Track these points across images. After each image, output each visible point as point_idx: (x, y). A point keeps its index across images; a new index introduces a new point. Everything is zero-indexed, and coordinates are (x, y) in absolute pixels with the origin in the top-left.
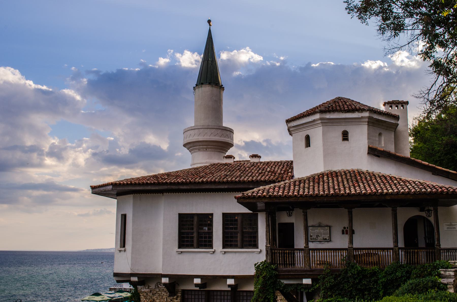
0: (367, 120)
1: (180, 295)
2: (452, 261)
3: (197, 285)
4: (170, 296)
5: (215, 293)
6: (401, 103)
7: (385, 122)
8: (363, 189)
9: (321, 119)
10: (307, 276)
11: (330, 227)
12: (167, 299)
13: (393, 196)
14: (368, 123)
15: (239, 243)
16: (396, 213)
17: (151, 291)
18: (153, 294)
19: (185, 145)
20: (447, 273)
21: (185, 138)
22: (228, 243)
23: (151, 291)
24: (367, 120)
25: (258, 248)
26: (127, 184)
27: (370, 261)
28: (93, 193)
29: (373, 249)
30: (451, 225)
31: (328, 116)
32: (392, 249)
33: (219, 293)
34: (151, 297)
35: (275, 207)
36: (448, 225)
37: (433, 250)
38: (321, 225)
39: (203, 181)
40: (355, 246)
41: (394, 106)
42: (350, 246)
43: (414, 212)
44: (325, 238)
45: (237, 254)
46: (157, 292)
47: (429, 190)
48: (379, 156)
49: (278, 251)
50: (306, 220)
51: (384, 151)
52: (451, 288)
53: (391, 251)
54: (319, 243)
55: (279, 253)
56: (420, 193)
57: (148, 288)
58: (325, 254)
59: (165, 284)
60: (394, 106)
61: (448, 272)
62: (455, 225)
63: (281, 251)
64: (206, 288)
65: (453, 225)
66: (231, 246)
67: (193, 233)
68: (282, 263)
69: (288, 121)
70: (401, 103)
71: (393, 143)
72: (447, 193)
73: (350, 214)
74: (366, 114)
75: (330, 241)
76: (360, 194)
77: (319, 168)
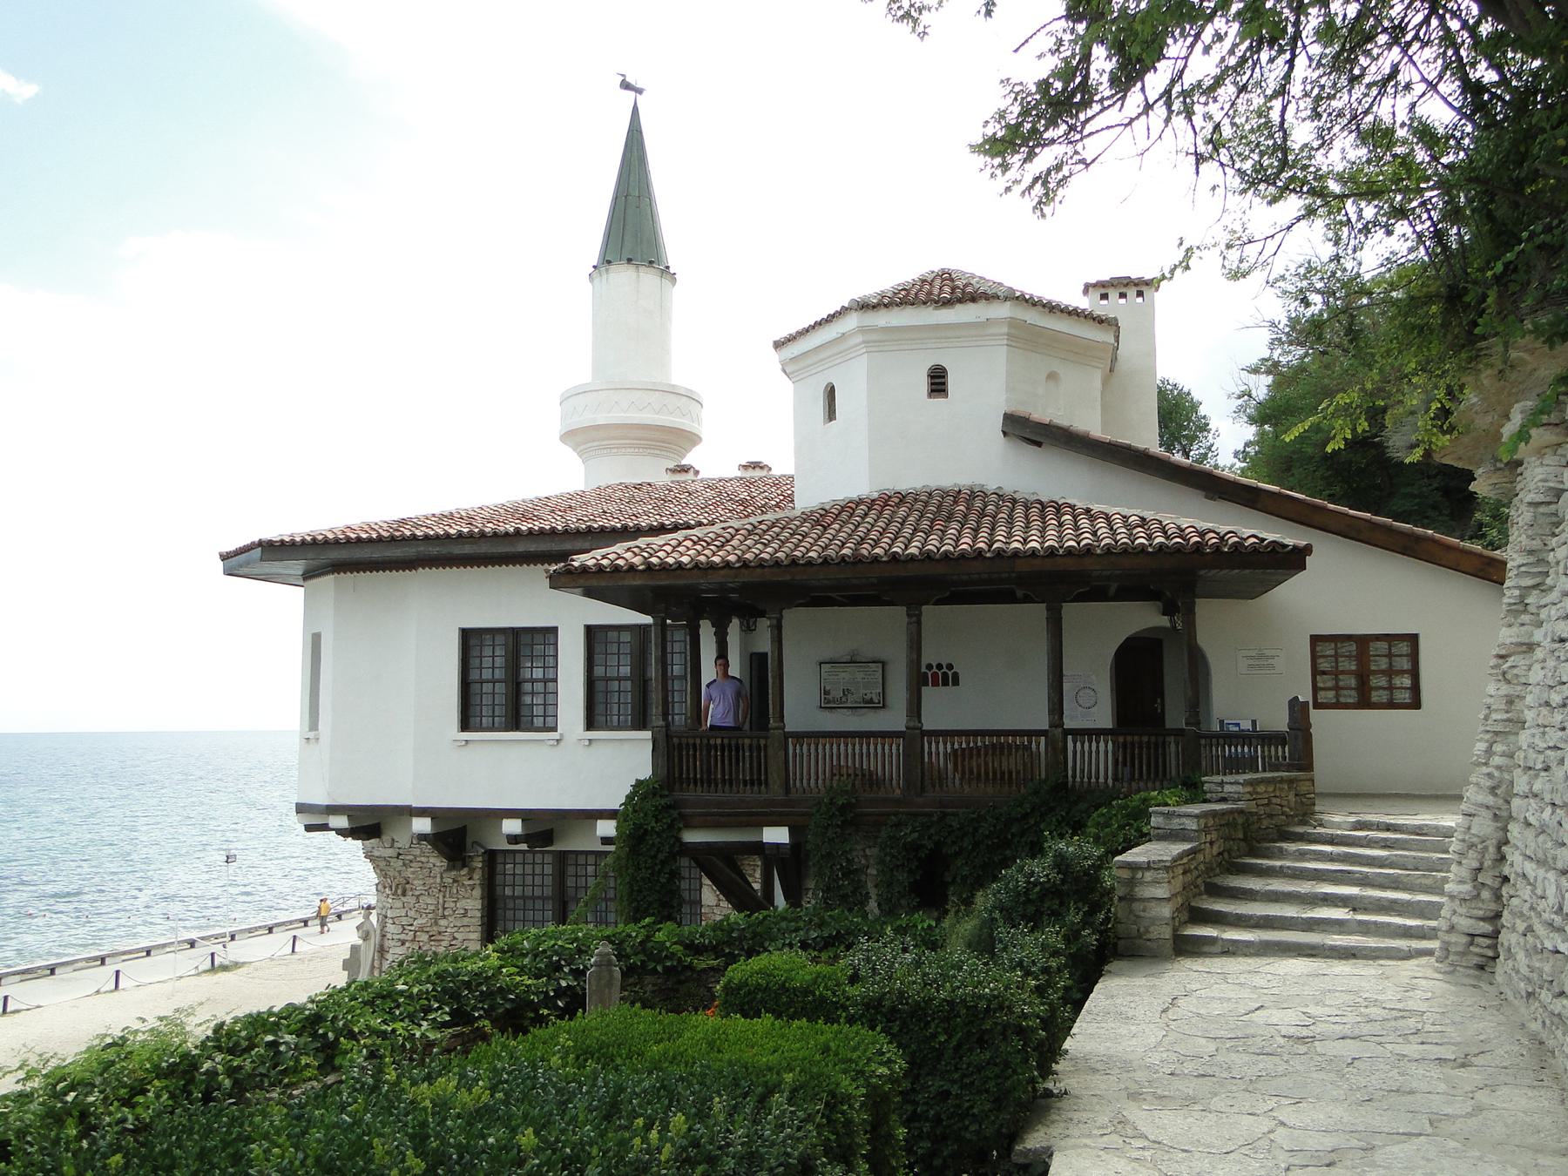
0: (1005, 330)
3: (513, 839)
4: (449, 869)
5: (581, 860)
9: (862, 330)
11: (884, 664)
13: (1037, 562)
24: (1005, 330)
26: (370, 540)
27: (1004, 767)
28: (229, 572)
29: (1015, 733)
30: (1261, 656)
31: (883, 319)
33: (591, 860)
35: (686, 599)
36: (1252, 657)
39: (518, 531)
40: (928, 725)
41: (1113, 294)
43: (1143, 617)
44: (868, 697)
45: (626, 746)
48: (1039, 444)
50: (915, 645)
51: (1110, 444)
52: (1156, 882)
56: (1129, 552)
59: (422, 837)
60: (1113, 294)
65: (1268, 658)
67: (498, 685)
69: (778, 345)
70: (1136, 285)
72: (1217, 549)
74: (1003, 311)
76: (928, 557)
77: (857, 484)
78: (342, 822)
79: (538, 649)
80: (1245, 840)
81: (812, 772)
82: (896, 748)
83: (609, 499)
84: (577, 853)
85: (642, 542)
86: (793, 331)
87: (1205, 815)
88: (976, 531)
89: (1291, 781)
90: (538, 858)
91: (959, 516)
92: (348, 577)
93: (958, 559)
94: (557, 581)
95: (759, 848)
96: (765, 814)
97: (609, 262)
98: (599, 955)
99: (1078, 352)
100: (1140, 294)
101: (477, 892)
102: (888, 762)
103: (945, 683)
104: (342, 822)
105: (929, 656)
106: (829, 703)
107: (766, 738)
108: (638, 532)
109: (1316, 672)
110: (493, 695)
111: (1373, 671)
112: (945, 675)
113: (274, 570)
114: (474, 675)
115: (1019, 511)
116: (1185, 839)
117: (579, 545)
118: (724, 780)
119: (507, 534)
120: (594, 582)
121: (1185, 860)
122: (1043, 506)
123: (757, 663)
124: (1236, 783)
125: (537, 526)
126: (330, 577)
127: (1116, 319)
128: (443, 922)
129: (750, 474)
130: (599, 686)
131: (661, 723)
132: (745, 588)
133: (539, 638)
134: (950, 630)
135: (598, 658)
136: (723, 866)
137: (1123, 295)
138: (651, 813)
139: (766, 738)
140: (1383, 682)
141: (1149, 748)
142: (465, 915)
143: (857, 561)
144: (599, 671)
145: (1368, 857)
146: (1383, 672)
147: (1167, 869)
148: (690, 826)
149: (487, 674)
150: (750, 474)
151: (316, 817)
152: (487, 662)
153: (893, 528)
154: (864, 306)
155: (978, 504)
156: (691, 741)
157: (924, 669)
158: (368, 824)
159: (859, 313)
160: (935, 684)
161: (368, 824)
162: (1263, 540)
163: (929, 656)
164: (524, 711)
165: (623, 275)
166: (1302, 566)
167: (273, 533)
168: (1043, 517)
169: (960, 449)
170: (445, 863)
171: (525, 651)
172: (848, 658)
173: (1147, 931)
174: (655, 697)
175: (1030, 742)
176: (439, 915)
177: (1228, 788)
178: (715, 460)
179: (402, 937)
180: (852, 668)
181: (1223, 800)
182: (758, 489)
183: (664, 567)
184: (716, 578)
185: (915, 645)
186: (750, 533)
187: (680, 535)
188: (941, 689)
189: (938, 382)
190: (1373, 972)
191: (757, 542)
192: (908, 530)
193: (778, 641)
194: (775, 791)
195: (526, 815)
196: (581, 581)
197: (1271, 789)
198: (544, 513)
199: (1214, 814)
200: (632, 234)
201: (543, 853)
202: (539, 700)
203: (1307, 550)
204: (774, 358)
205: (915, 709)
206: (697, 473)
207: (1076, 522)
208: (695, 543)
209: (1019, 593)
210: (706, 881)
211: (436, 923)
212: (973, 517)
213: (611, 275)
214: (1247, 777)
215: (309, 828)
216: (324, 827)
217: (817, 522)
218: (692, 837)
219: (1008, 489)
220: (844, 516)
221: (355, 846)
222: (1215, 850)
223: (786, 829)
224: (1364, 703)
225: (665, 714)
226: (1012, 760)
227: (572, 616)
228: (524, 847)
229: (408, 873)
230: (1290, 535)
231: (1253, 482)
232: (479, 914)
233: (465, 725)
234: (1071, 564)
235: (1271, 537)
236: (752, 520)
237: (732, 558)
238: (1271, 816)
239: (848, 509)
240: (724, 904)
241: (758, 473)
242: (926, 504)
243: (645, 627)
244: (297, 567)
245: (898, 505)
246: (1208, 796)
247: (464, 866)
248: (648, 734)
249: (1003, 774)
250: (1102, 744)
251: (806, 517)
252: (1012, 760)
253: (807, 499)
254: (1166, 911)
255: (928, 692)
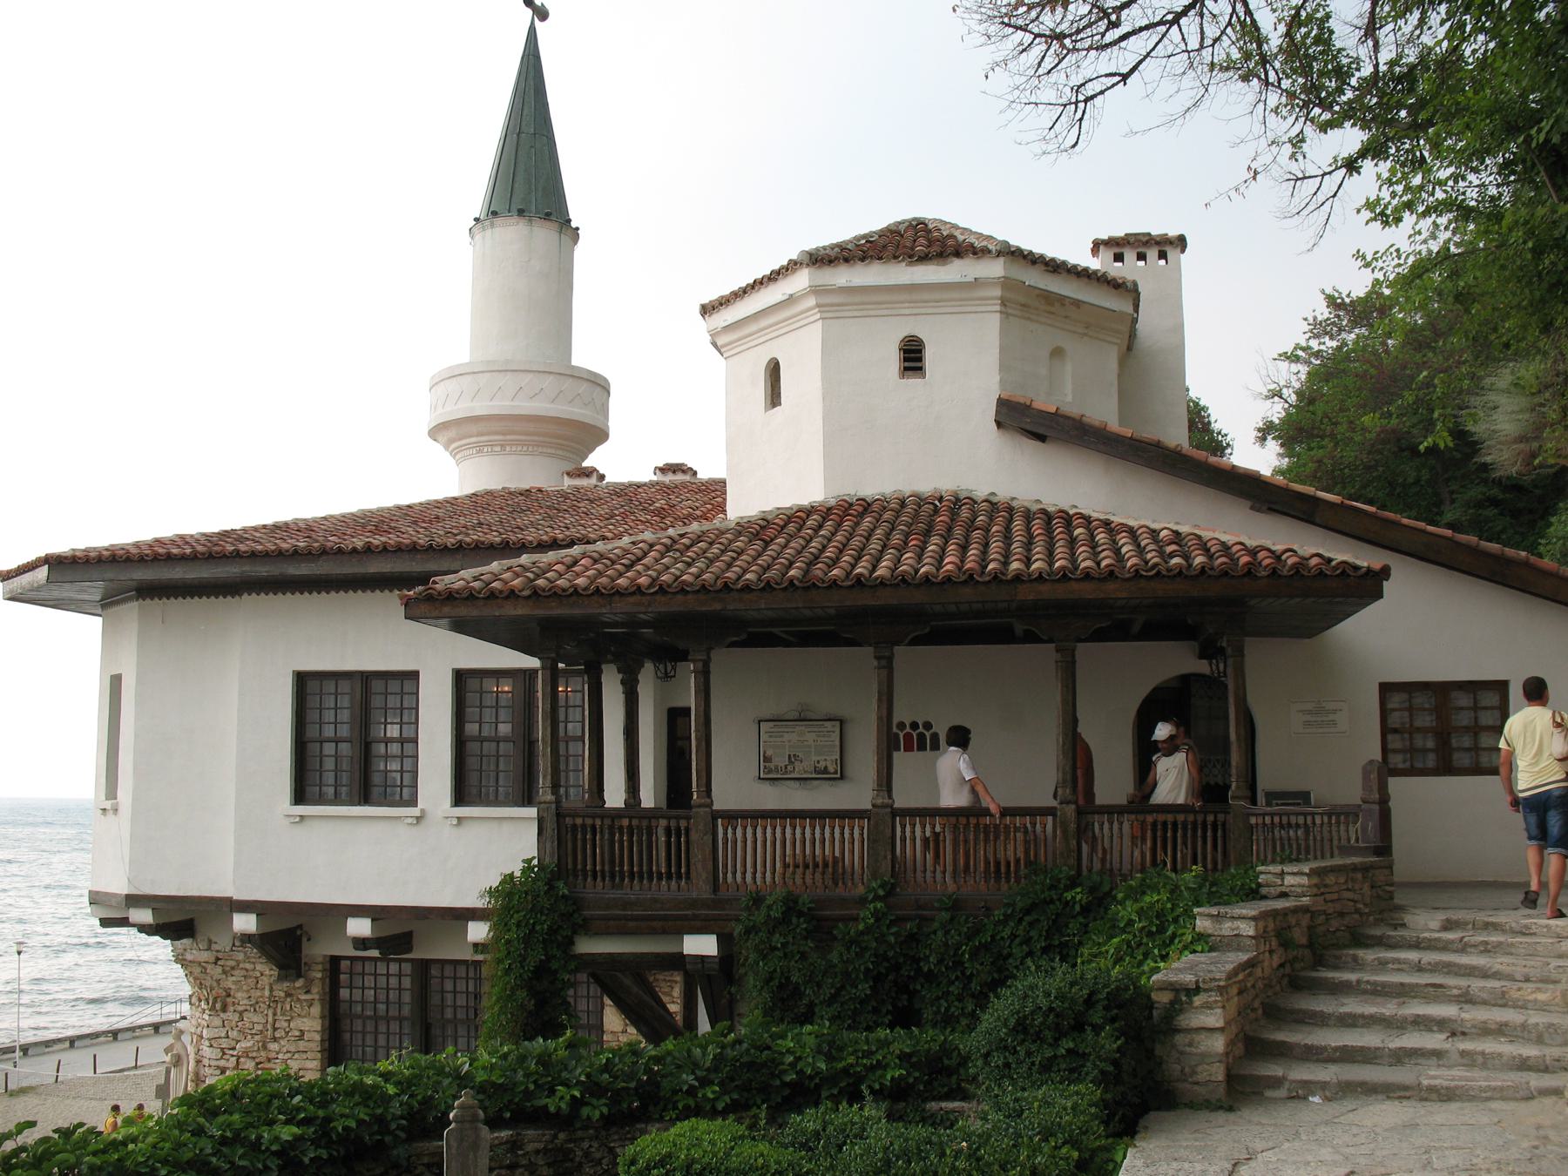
0: (998, 292)
1: (319, 975)
2: (1271, 868)
3: (361, 943)
4: (280, 979)
5: (448, 970)
6: (1158, 243)
7: (1077, 303)
8: (942, 559)
10: (698, 924)
11: (842, 722)
12: (271, 990)
14: (1003, 304)
15: (492, 797)
16: (1074, 662)
17: (218, 959)
18: (224, 972)
19: (435, 432)
20: (1227, 928)
21: (434, 408)
22: (466, 789)
23: (218, 959)
25: (413, 802)
27: (1001, 855)
31: (844, 276)
32: (1050, 811)
34: (218, 981)
36: (1310, 712)
37: (1221, 817)
38: (810, 715)
40: (900, 802)
42: (879, 801)
43: (1175, 660)
44: (822, 765)
45: (506, 827)
46: (238, 962)
47: (1199, 560)
48: (1041, 438)
49: (589, 821)
50: (887, 699)
52: (1208, 1006)
53: (1050, 818)
54: (796, 784)
55: (594, 827)
57: (209, 949)
58: (778, 835)
59: (246, 938)
61: (1228, 924)
62: (1334, 712)
63: (598, 822)
64: (410, 950)
66: (321, 800)
67: (342, 747)
68: (603, 871)
69: (707, 310)
70: (1158, 243)
71: (1115, 389)
73: (887, 664)
75: (842, 777)
77: (805, 486)
78: (145, 916)
79: (393, 701)
80: (1310, 945)
81: (753, 863)
82: (858, 831)
83: (486, 507)
84: (443, 962)
85: (525, 559)
86: (726, 292)
87: (1264, 916)
88: (964, 548)
89: (1365, 869)
90: (394, 968)
91: (940, 528)
92: (155, 605)
93: (942, 583)
94: (417, 610)
95: (678, 961)
96: (686, 918)
97: (495, 213)
98: (461, 1107)
99: (1091, 323)
100: (1163, 255)
101: (316, 1010)
102: (851, 846)
103: (922, 747)
104: (145, 916)
105: (902, 714)
106: (771, 774)
107: (688, 818)
108: (523, 548)
109: (1385, 731)
110: (334, 755)
111: (1447, 726)
112: (921, 737)
113: (65, 595)
114: (312, 732)
115: (1018, 525)
116: (1239, 949)
117: (445, 564)
118: (632, 874)
119: (354, 550)
120: (463, 611)
121: (1240, 977)
122: (1048, 517)
123: (675, 719)
124: (1300, 873)
125: (392, 539)
126: (134, 605)
127: (1135, 284)
128: (274, 1046)
129: (669, 478)
130: (472, 747)
131: (550, 797)
132: (664, 622)
133: (394, 686)
134: (932, 682)
135: (472, 712)
136: (629, 984)
137: (1141, 257)
138: (538, 911)
139: (688, 818)
140: (1467, 742)
141: (1185, 829)
142: (301, 1037)
143: (808, 586)
144: (471, 729)
145: (1466, 967)
146: (1467, 729)
147: (1221, 990)
148: (587, 928)
149: (329, 731)
150: (669, 478)
151: (114, 913)
152: (329, 716)
153: (856, 542)
154: (819, 259)
155: (965, 513)
156: (589, 821)
157: (895, 730)
158: (179, 920)
159: (812, 269)
160: (909, 748)
161: (179, 920)
162: (1330, 560)
163: (902, 714)
164: (377, 779)
165: (512, 232)
166: (1378, 595)
167: (61, 547)
168: (1049, 531)
169: (947, 443)
170: (276, 973)
171: (377, 701)
172: (795, 715)
173: (1194, 1072)
174: (543, 764)
175: (1034, 824)
176: (269, 1036)
177: (1289, 880)
178: (623, 460)
179: (222, 1063)
180: (801, 727)
181: (1284, 895)
182: (683, 494)
183: (556, 595)
184: (622, 607)
185: (887, 699)
186: (668, 549)
187: (576, 550)
188: (916, 754)
189: (912, 357)
190: (1485, 1120)
191: (676, 561)
192: (874, 546)
193: (705, 693)
194: (700, 888)
195: (376, 913)
196: (446, 610)
197: (1342, 880)
198: (402, 525)
199: (1274, 914)
200: (529, 180)
201: (400, 961)
202: (394, 766)
203: (1385, 572)
204: (701, 328)
205: (885, 782)
206: (602, 477)
207: (1092, 537)
208: (595, 561)
209: (1019, 628)
210: (607, 1001)
211: (265, 1047)
212: (958, 532)
213: (497, 230)
214: (1315, 865)
215: (106, 923)
216: (124, 922)
217: (756, 535)
218: (588, 946)
219: (1004, 493)
220: (791, 528)
221: (161, 948)
222: (1276, 960)
223: (713, 938)
224: (1446, 768)
225: (555, 787)
226: (1011, 847)
227: (436, 656)
228: (375, 953)
229: (229, 983)
230: (1365, 558)
231: (1309, 490)
232: (318, 1037)
233: (300, 797)
234: (1087, 591)
235: (1339, 556)
236: (671, 532)
237: (643, 580)
238: (1342, 914)
239: (797, 518)
240: (632, 1030)
241: (680, 477)
242: (898, 513)
243: (534, 672)
244: (94, 591)
245: (861, 515)
246: (1264, 891)
247: (299, 976)
248: (532, 812)
249: (998, 864)
250: (749, 830)
251: (742, 528)
252: (1011, 847)
253: (742, 506)
254: (1218, 1044)
255: (899, 757)
